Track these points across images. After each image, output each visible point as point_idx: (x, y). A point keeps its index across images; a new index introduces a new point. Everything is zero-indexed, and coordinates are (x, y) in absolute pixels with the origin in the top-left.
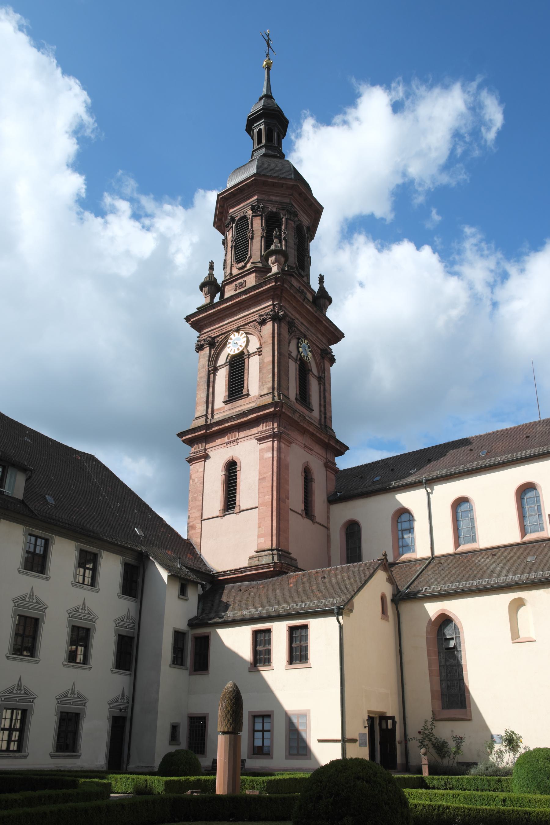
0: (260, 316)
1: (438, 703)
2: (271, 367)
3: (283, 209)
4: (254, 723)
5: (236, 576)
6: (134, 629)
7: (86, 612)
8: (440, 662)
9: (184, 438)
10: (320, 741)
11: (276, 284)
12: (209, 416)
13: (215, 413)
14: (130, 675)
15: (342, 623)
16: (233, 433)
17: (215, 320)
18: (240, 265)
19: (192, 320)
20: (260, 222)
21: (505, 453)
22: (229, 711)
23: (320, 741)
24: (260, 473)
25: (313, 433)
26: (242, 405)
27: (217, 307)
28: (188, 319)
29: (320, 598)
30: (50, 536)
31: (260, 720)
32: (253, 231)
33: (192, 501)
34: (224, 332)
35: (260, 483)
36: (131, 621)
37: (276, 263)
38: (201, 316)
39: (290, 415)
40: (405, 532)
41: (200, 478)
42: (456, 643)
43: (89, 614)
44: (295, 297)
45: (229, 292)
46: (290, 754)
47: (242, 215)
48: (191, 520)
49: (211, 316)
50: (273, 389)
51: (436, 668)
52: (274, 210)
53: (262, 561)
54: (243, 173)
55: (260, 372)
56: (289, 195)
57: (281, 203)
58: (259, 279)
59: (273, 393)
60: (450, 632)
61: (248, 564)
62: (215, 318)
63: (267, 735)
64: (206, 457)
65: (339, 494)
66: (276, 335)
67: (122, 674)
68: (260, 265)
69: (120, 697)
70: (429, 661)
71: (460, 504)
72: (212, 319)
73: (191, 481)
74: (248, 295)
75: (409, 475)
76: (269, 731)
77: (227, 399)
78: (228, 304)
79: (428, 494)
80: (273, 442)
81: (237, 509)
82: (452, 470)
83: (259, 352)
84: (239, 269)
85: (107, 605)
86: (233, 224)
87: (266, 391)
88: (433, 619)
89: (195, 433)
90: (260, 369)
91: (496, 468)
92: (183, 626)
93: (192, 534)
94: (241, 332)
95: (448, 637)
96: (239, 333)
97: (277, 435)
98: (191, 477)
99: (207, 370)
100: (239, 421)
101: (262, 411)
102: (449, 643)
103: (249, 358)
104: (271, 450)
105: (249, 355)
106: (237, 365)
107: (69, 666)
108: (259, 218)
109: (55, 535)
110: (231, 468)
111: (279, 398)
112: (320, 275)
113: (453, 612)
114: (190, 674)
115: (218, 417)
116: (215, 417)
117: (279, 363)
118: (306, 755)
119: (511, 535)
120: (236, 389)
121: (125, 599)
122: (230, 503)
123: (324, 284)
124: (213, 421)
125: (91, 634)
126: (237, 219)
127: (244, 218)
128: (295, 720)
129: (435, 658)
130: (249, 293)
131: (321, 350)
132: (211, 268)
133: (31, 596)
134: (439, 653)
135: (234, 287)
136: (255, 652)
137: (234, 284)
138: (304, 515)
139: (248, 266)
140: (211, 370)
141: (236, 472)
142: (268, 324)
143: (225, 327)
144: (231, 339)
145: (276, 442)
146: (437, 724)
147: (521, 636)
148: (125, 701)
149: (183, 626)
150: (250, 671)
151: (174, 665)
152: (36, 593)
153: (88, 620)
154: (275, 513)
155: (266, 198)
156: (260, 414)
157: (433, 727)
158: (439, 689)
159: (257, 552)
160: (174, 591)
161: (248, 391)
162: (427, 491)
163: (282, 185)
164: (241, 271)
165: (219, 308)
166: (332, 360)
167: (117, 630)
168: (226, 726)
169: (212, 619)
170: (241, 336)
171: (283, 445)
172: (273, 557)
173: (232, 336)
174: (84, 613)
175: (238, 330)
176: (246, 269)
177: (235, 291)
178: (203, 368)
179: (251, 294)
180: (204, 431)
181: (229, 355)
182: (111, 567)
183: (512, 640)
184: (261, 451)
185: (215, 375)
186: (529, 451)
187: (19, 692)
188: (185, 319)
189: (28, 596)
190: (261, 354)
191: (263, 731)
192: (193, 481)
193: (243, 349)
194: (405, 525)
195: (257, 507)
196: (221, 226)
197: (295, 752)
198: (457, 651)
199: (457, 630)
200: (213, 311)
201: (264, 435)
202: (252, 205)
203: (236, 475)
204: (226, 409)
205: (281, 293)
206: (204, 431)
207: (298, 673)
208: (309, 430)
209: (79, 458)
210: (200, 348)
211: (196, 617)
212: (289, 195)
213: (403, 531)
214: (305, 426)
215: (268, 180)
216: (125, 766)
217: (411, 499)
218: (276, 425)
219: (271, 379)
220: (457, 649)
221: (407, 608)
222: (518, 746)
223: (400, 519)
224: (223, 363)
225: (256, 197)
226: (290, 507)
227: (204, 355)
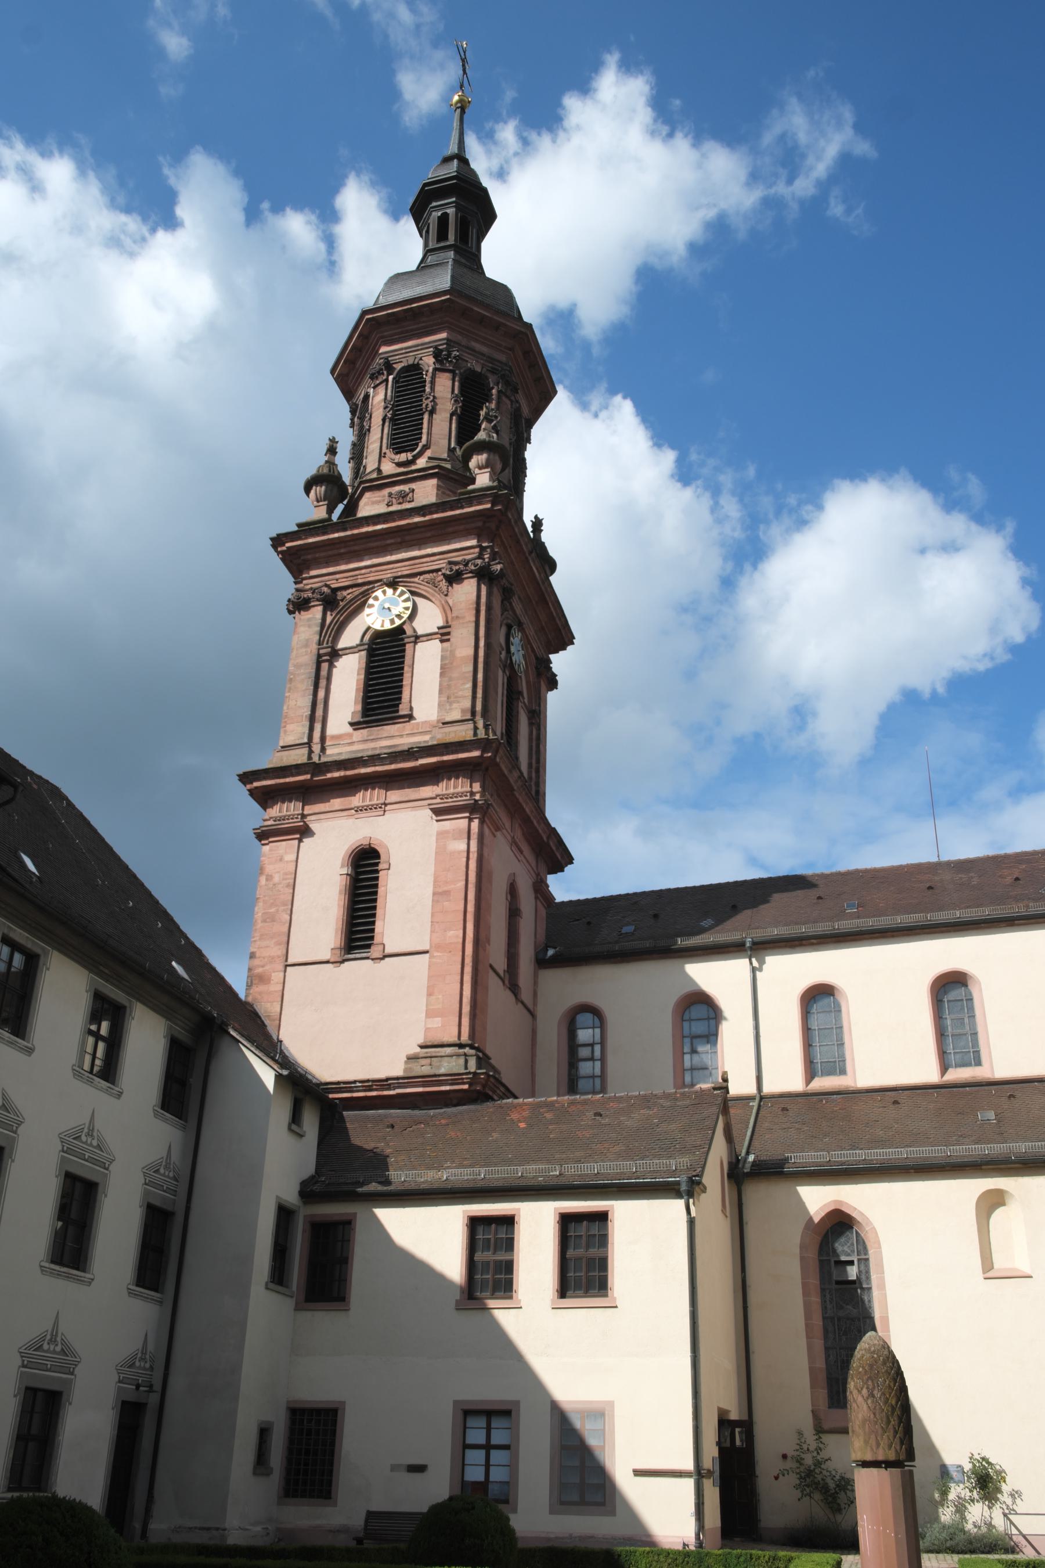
0: (450, 563)
2: (471, 668)
3: (493, 371)
4: (465, 1428)
5: (374, 1093)
6: (175, 1193)
8: (824, 1309)
9: (256, 784)
10: (638, 1473)
11: (493, 505)
12: (317, 748)
13: (328, 743)
14: (160, 1303)
15: (693, 1214)
16: (373, 789)
17: (341, 554)
18: (403, 457)
19: (288, 545)
20: (449, 383)
22: (893, 1409)
23: (638, 1473)
24: (435, 881)
25: (529, 818)
27: (352, 529)
28: (277, 541)
29: (619, 1156)
30: (43, 949)
31: (482, 1422)
32: (434, 397)
33: (264, 921)
34: (360, 581)
35: (435, 902)
36: (171, 1175)
37: (486, 467)
38: (311, 540)
39: (506, 772)
40: (698, 1040)
41: (286, 874)
42: (860, 1272)
43: (99, 1147)
44: (518, 542)
45: (370, 505)
46: (562, 1503)
47: (411, 362)
48: (256, 962)
49: (334, 544)
50: (473, 713)
51: (818, 1321)
52: (478, 369)
53: (439, 1067)
54: (419, 284)
55: (442, 674)
57: (491, 359)
58: (443, 493)
59: (473, 719)
60: (846, 1248)
61: (405, 1070)
62: (342, 551)
63: (496, 1456)
64: (304, 832)
65: (551, 952)
66: (483, 608)
67: (146, 1299)
68: (448, 466)
69: (139, 1355)
70: (807, 1306)
71: (818, 997)
72: (335, 552)
73: (263, 880)
74: (427, 518)
75: (703, 931)
76: (506, 1447)
77: (358, 718)
78: (379, 527)
79: (754, 970)
80: (470, 820)
81: (375, 951)
82: (803, 930)
83: (444, 634)
84: (399, 464)
85: (132, 1134)
86: (389, 374)
87: (456, 715)
88: (816, 1220)
89: (285, 777)
90: (442, 668)
91: (893, 936)
92: (291, 1196)
93: (260, 993)
94: (400, 589)
95: (843, 1258)
96: (395, 590)
97: (481, 807)
98: (261, 870)
99: (315, 652)
100: (393, 767)
101: (453, 753)
102: (845, 1271)
103: (415, 643)
104: (466, 836)
105: (417, 638)
106: (388, 654)
107: (53, 1274)
108: (448, 375)
109: (54, 948)
110: (365, 863)
111: (487, 733)
112: (536, 517)
114: (298, 1308)
115: (334, 753)
116: (329, 752)
117: (486, 663)
118: (603, 1504)
119: (920, 1067)
120: (382, 698)
121: (165, 1120)
122: (359, 932)
123: (543, 535)
124: (324, 759)
125: (98, 1198)
126: (398, 367)
127: (414, 370)
128: (577, 1424)
129: (816, 1299)
130: (432, 513)
131: (537, 658)
132: (332, 450)
134: (823, 1290)
135: (387, 499)
136: (472, 1265)
137: (386, 492)
139: (421, 463)
140: (325, 655)
141: (377, 871)
142: (466, 582)
143: (363, 571)
144: (376, 599)
145: (476, 821)
146: (827, 1438)
147: (996, 1266)
148: (147, 1365)
149: (291, 1196)
150: (459, 1307)
153: (95, 1162)
154: (468, 969)
155: (464, 342)
156: (445, 758)
157: (821, 1446)
158: (824, 1366)
159: (422, 1047)
160: (280, 1113)
161: (411, 709)
162: (751, 963)
163: (497, 327)
164: (402, 470)
165: (356, 532)
166: (552, 683)
167: (146, 1193)
168: (890, 1447)
169: (362, 1184)
170: (400, 595)
171: (486, 830)
172: (466, 1062)
173: (379, 593)
175: (393, 584)
176: (413, 467)
177: (388, 505)
178: (306, 646)
179: (435, 516)
180: (308, 777)
181: (369, 628)
182: (147, 1039)
183: (984, 1273)
184: (441, 835)
185: (331, 666)
186: (958, 913)
188: (272, 539)
190: (448, 640)
191: (488, 1447)
192: (269, 878)
193: (404, 623)
194: (699, 1028)
195: (427, 952)
196: (347, 375)
198: (862, 1289)
199: (862, 1247)
200: (342, 534)
201: (450, 803)
202: (436, 347)
203: (377, 878)
204: (355, 739)
206: (308, 777)
207: (582, 1317)
208: (524, 810)
209: (35, 787)
210: (298, 605)
211: (312, 1177)
213: (694, 1037)
214: (521, 800)
215: (475, 309)
216: (138, 1526)
217: (718, 977)
218: (477, 787)
219: (469, 693)
220: (861, 1283)
221: (761, 1196)
222: (999, 1490)
223: (687, 1013)
224: (354, 644)
225: (444, 335)
226: (491, 962)
227: (309, 620)
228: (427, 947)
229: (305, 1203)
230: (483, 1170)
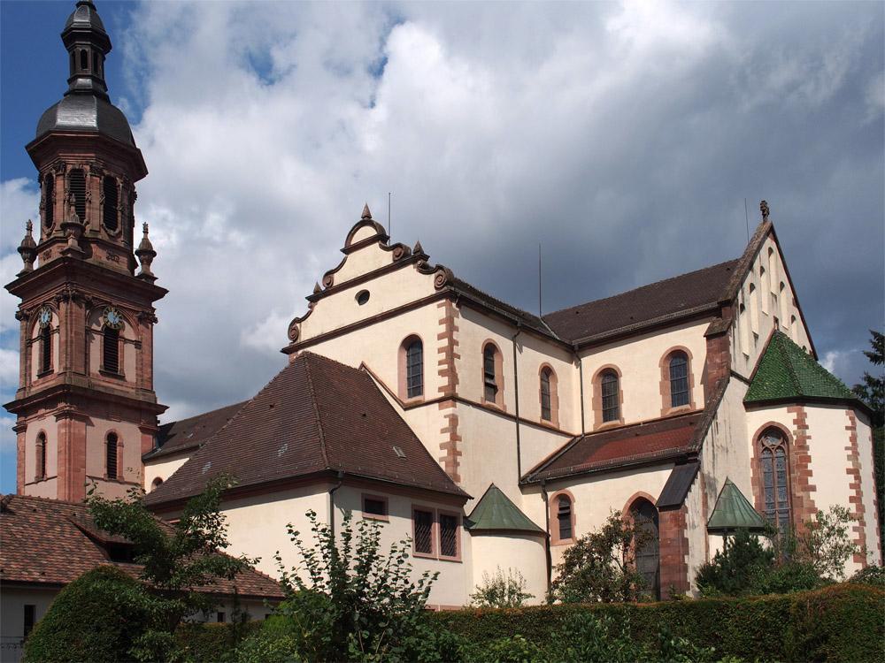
26: (51, 382)
184: (59, 426)
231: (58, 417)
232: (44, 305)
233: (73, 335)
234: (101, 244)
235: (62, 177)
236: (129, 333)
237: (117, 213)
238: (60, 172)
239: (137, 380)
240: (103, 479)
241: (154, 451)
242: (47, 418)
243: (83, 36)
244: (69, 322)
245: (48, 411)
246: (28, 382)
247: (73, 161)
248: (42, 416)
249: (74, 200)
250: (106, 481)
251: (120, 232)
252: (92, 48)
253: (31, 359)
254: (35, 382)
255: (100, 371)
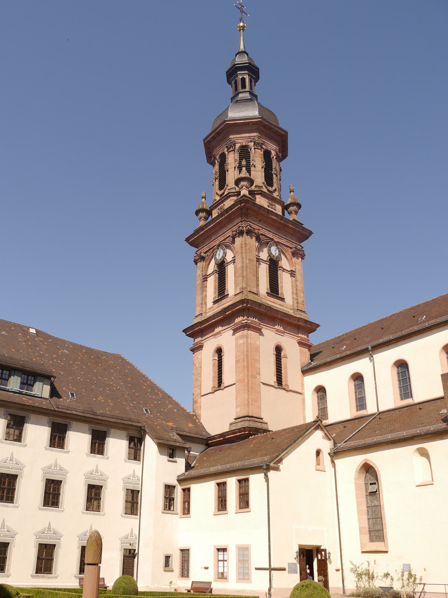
1: (367, 537)
7: (99, 474)
10: (257, 569)
21: (437, 317)
23: (257, 569)
24: (236, 356)
26: (226, 303)
28: (187, 240)
46: (239, 579)
48: (194, 396)
56: (255, 129)
83: (234, 261)
87: (238, 291)
91: (424, 332)
107: (87, 514)
113: (373, 461)
118: (248, 579)
133: (56, 465)
138: (276, 386)
151: (165, 511)
152: (59, 463)
174: (98, 475)
176: (225, 194)
184: (237, 339)
187: (49, 532)
189: (53, 465)
197: (242, 577)
205: (247, 211)
212: (255, 129)
228: (234, 382)
229: (180, 483)
230: (266, 457)
231: (235, 331)
232: (219, 245)
233: (247, 261)
234: (262, 194)
235: (232, 152)
236: (284, 263)
237: (272, 176)
238: (231, 149)
239: (293, 302)
240: (273, 386)
241: (310, 364)
242: (223, 334)
243: (242, 68)
244: (244, 251)
245: (224, 328)
246: (204, 309)
247: (241, 139)
248: (219, 333)
249: (245, 163)
250: (277, 388)
251: (275, 190)
252: (249, 75)
253: (206, 291)
254: (210, 309)
255: (267, 293)
